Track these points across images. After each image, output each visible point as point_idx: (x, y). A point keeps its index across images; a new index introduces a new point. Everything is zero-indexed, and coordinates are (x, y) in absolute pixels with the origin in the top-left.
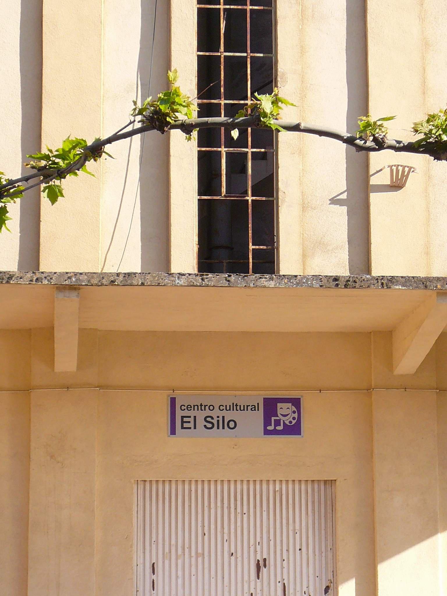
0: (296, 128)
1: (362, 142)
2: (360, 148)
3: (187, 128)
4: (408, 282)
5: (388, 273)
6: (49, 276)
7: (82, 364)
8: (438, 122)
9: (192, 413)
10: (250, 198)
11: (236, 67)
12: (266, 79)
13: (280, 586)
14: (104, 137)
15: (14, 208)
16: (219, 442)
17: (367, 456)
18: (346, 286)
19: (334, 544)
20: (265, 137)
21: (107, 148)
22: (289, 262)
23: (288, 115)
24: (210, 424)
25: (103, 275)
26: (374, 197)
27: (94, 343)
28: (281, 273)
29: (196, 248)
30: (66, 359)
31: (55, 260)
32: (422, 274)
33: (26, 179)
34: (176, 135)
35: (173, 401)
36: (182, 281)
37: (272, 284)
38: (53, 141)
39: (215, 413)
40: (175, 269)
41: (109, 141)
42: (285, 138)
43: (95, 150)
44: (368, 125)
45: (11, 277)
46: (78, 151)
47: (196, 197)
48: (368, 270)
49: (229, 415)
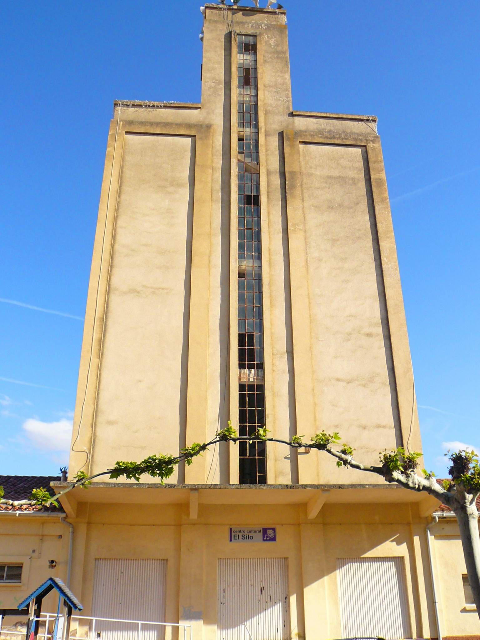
0: (271, 440)
1: (295, 445)
2: (293, 446)
3: (235, 440)
4: (311, 486)
5: (305, 483)
6: (188, 485)
7: (199, 516)
8: (319, 437)
9: (237, 534)
10: (257, 457)
11: (252, 412)
12: (262, 423)
13: (269, 597)
14: (206, 443)
15: (176, 467)
16: (247, 544)
17: (299, 549)
18: (290, 488)
19: (288, 580)
20: (263, 444)
21: (207, 447)
22: (271, 480)
23: (269, 436)
24: (244, 538)
25: (206, 485)
26: (299, 456)
27: (204, 509)
28: (268, 483)
29: (238, 475)
30: (194, 515)
31: (190, 480)
32: (316, 484)
33: (180, 457)
34: (231, 442)
35: (231, 529)
36: (234, 487)
37: (265, 487)
38: (189, 445)
39: (246, 533)
40: (231, 483)
41: (208, 444)
42: (268, 442)
43: (203, 448)
44: (296, 438)
45: (175, 486)
46: (198, 448)
47: (238, 457)
48: (298, 482)
49: (250, 534)
